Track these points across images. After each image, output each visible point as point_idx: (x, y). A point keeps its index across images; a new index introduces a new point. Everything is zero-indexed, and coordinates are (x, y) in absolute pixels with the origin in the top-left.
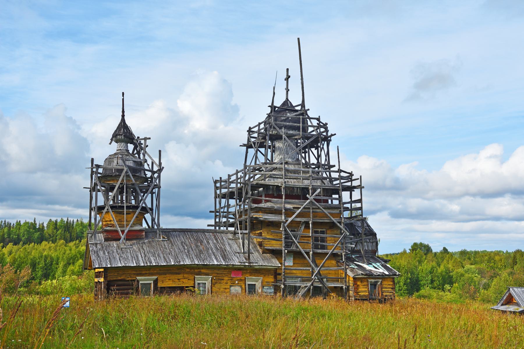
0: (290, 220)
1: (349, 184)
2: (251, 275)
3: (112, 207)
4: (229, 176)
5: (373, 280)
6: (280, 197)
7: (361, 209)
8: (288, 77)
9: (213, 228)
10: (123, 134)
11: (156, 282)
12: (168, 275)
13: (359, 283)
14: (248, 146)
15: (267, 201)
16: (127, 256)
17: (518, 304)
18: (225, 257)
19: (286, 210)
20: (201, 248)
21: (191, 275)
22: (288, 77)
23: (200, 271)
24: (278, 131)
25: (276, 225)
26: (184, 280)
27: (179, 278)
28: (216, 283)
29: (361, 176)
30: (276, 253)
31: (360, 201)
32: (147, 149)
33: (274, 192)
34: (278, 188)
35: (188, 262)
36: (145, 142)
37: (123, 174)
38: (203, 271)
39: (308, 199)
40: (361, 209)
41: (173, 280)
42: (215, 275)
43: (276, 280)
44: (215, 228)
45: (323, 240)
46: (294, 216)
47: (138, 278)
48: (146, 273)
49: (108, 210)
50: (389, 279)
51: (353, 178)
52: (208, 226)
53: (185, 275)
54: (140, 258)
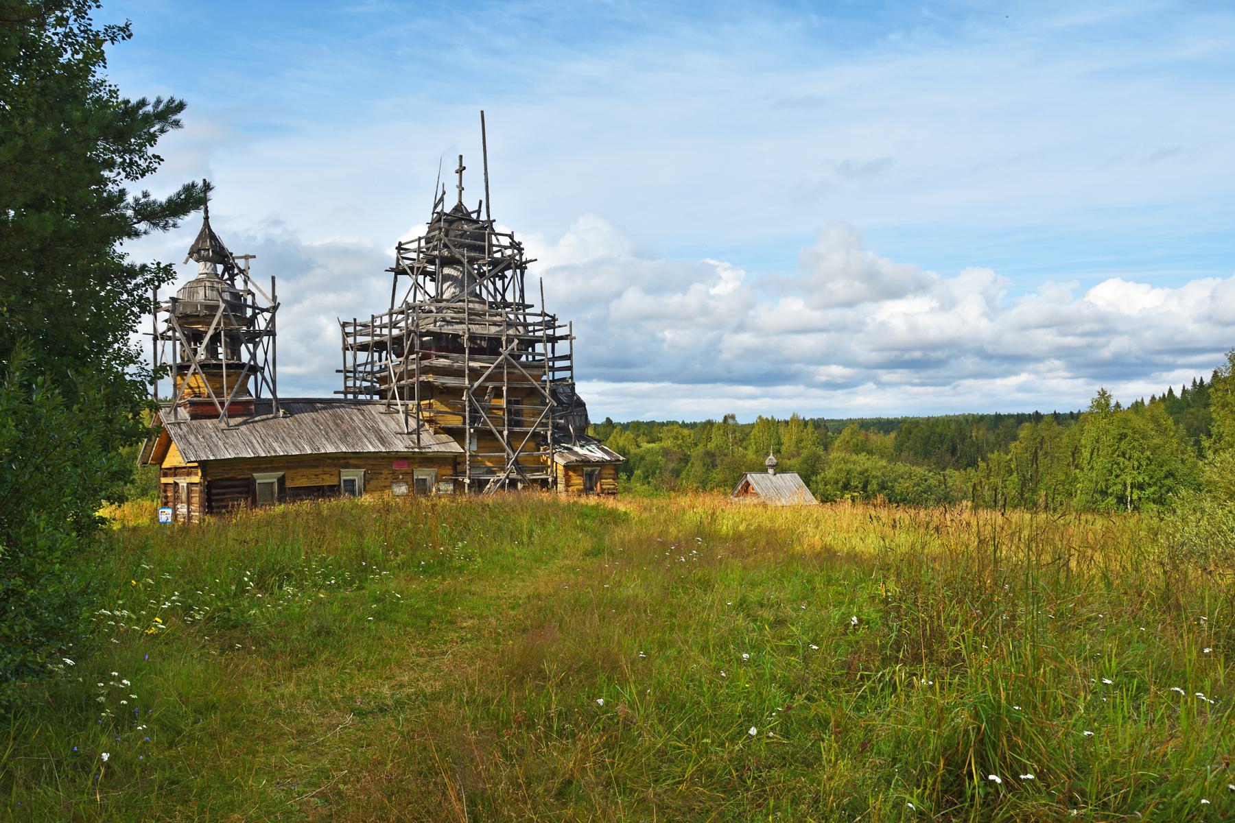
0: (476, 384)
1: (550, 332)
3: (203, 366)
6: (462, 351)
7: (570, 368)
8: (461, 170)
11: (282, 481)
13: (571, 473)
15: (438, 357)
16: (239, 443)
17: (756, 494)
18: (382, 440)
19: (471, 369)
20: (344, 427)
22: (461, 170)
26: (324, 477)
30: (457, 434)
33: (448, 344)
34: (456, 336)
35: (331, 449)
36: (247, 263)
37: (219, 314)
38: (352, 461)
39: (500, 354)
40: (570, 368)
41: (311, 478)
43: (456, 473)
46: (482, 379)
47: (255, 475)
51: (557, 324)
53: (326, 469)
54: (257, 445)
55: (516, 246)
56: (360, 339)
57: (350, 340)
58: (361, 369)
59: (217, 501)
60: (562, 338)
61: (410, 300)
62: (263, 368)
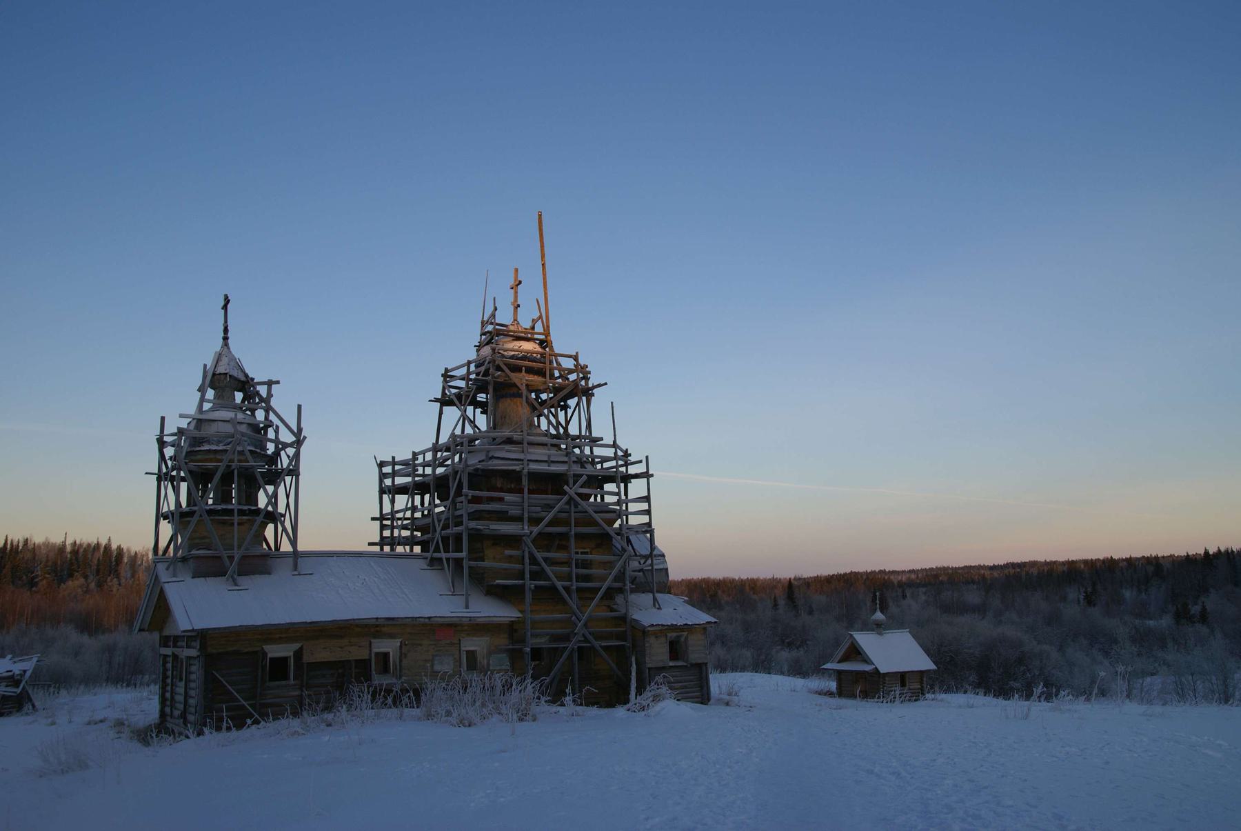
4: (415, 454)
5: (674, 634)
9: (377, 549)
24: (507, 375)
25: (513, 541)
31: (647, 499)
32: (273, 403)
44: (382, 549)
47: (267, 648)
51: (632, 459)
52: (370, 544)
57: (388, 482)
60: (637, 476)
61: (458, 432)
62: (284, 516)
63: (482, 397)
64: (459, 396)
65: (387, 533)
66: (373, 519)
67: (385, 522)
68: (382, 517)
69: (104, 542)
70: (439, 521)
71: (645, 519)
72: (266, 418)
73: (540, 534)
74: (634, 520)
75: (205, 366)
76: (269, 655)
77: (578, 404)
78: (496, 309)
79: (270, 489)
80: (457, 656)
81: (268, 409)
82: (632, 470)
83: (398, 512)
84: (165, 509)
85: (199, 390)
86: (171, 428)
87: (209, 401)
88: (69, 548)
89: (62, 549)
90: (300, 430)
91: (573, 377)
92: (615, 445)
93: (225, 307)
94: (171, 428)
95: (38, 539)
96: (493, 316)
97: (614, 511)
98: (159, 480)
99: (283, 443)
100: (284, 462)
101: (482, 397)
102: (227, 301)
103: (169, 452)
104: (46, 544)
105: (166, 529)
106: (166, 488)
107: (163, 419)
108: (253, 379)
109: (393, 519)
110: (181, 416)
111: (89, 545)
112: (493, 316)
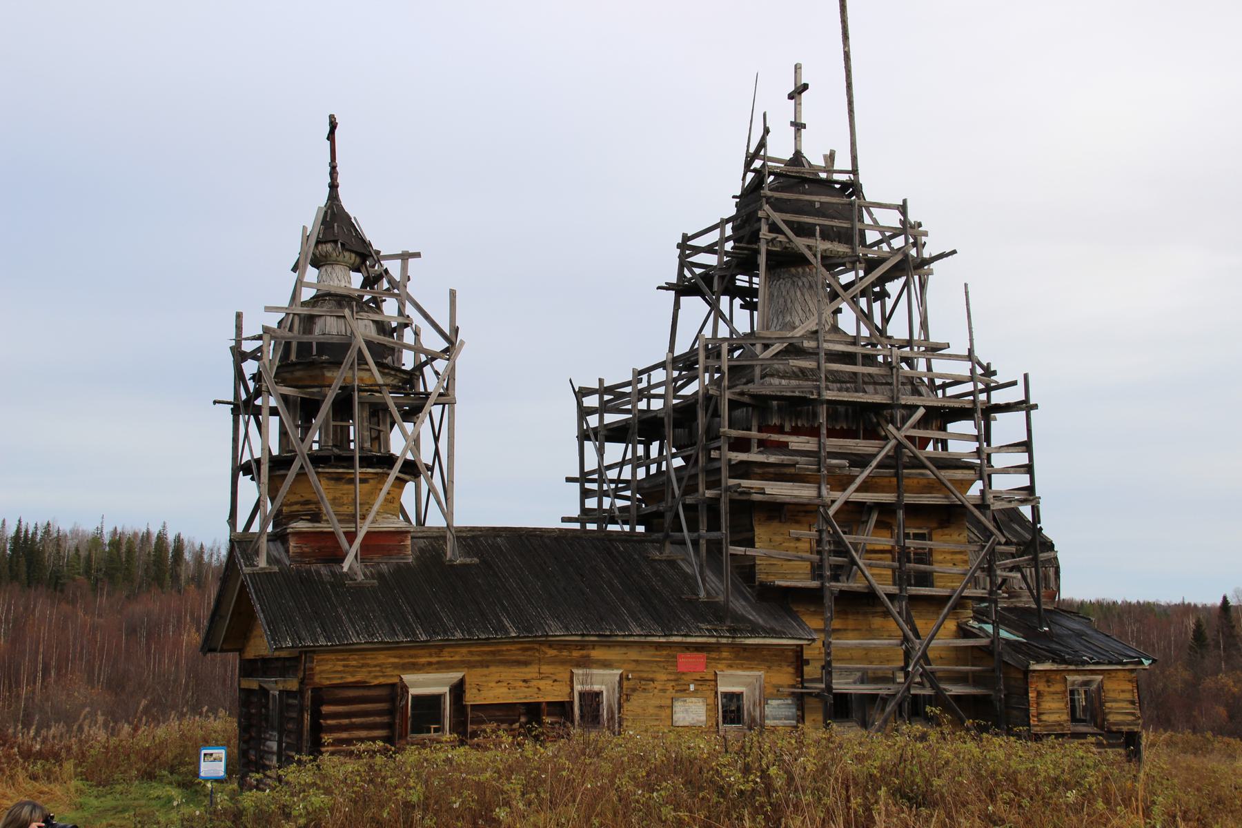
2: (730, 666)
9: (577, 526)
10: (336, 237)
12: (493, 669)
14: (683, 289)
21: (561, 668)
23: (588, 656)
26: (542, 684)
27: (528, 677)
28: (634, 690)
29: (1026, 376)
31: (1027, 446)
32: (411, 288)
36: (404, 269)
42: (632, 666)
45: (924, 557)
47: (408, 678)
48: (430, 664)
49: (302, 467)
50: (1121, 674)
52: (564, 520)
53: (546, 669)
55: (908, 228)
56: (610, 418)
57: (593, 421)
58: (612, 474)
59: (332, 729)
60: (1007, 408)
61: (707, 332)
62: (431, 469)
63: (742, 281)
64: (707, 278)
65: (592, 503)
66: (569, 480)
67: (588, 486)
68: (584, 477)
69: (155, 531)
70: (679, 480)
71: (1024, 480)
72: (401, 313)
73: (846, 503)
74: (1001, 483)
75: (305, 228)
76: (413, 691)
77: (906, 284)
78: (767, 131)
79: (409, 427)
80: (711, 701)
81: (403, 299)
82: (998, 397)
83: (610, 467)
84: (246, 457)
85: (295, 269)
86: (252, 328)
87: (309, 285)
88: (107, 539)
89: (96, 541)
90: (456, 330)
91: (898, 242)
92: (970, 356)
93: (331, 136)
94: (252, 328)
95: (64, 525)
96: (762, 144)
97: (970, 467)
98: (236, 412)
99: (426, 352)
100: (431, 382)
101: (742, 281)
102: (333, 126)
103: (250, 367)
104: (75, 533)
105: (249, 490)
106: (247, 424)
107: (239, 316)
108: (378, 252)
109: (601, 481)
110: (268, 309)
111: (135, 534)
112: (762, 144)
